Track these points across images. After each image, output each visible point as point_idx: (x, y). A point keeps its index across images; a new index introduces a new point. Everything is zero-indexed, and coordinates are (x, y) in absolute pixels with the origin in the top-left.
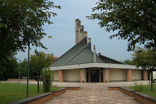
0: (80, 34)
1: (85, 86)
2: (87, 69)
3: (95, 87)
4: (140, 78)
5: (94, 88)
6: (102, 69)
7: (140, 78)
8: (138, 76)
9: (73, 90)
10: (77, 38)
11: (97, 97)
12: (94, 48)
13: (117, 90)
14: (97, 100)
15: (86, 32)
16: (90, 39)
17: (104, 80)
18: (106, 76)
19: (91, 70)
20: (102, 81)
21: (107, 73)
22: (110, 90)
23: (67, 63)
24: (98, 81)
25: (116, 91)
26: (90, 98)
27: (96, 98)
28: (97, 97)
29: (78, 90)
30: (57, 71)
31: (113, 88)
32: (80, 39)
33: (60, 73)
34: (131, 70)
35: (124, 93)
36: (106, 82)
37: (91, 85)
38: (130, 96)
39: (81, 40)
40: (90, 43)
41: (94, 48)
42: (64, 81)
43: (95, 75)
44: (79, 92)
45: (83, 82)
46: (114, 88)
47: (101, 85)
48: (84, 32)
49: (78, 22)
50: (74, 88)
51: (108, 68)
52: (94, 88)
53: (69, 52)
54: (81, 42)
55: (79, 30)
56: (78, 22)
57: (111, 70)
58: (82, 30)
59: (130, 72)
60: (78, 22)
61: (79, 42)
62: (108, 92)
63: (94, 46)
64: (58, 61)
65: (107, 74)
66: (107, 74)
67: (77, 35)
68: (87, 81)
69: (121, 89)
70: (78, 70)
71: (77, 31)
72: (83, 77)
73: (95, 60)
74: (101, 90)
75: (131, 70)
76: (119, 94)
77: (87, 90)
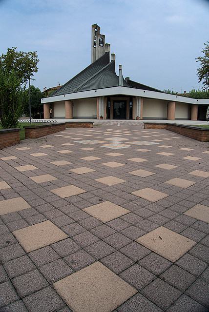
0: (98, 48)
1: (104, 122)
2: (108, 98)
3: (120, 124)
4: (186, 117)
5: (119, 126)
6: (132, 98)
7: (185, 116)
8: (184, 115)
9: (79, 127)
10: (94, 54)
11: (127, 139)
12: (120, 70)
13: (162, 129)
14: (128, 146)
15: (108, 45)
16: (114, 55)
17: (134, 116)
18: (138, 110)
19: (115, 101)
20: (131, 118)
21: (139, 105)
22: (149, 128)
23: (79, 89)
24: (123, 117)
25: (161, 130)
26: (109, 142)
27: (123, 142)
28: (127, 139)
29: (89, 127)
30: (62, 103)
31: (155, 126)
32: (99, 55)
33: (67, 105)
34: (175, 103)
35: (179, 134)
36: (138, 118)
37: (113, 122)
38: (201, 141)
39: (100, 57)
40: (114, 62)
41: (120, 70)
42: (73, 118)
43: (120, 108)
44: (90, 131)
45: (102, 118)
46: (157, 126)
47: (130, 123)
48: (104, 45)
49: (96, 30)
50: (82, 124)
51: (142, 97)
52: (119, 126)
53: (82, 75)
54: (100, 59)
55: (97, 42)
56: (95, 46)
57: (145, 100)
58: (103, 42)
59: (173, 106)
60: (95, 27)
61: (97, 59)
62: (146, 132)
63: (120, 66)
64: (65, 88)
65: (140, 106)
66: (140, 106)
67: (93, 50)
68: (108, 118)
69: (169, 127)
70: (93, 100)
71: (95, 44)
72: (101, 109)
73: (121, 83)
74: (131, 128)
75: (175, 103)
76: (163, 137)
77: (106, 128)
